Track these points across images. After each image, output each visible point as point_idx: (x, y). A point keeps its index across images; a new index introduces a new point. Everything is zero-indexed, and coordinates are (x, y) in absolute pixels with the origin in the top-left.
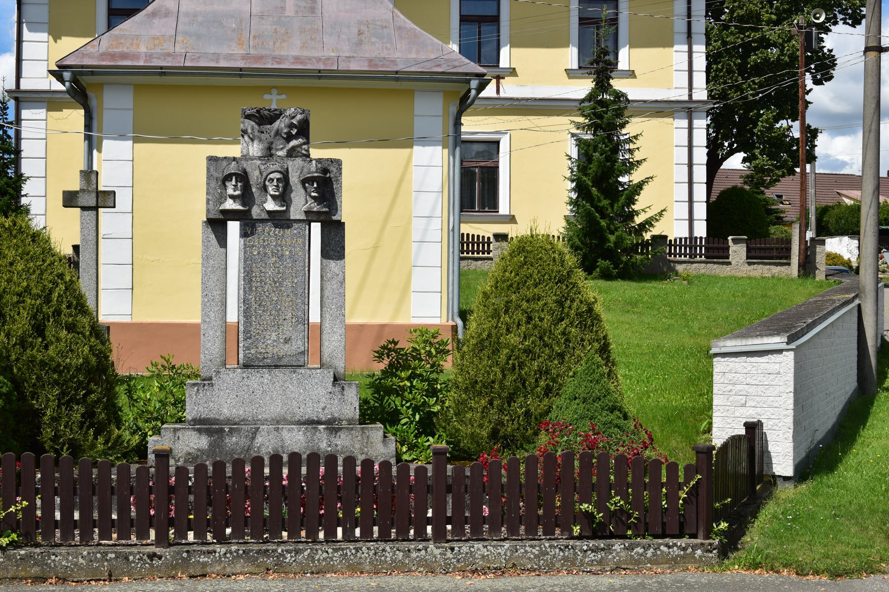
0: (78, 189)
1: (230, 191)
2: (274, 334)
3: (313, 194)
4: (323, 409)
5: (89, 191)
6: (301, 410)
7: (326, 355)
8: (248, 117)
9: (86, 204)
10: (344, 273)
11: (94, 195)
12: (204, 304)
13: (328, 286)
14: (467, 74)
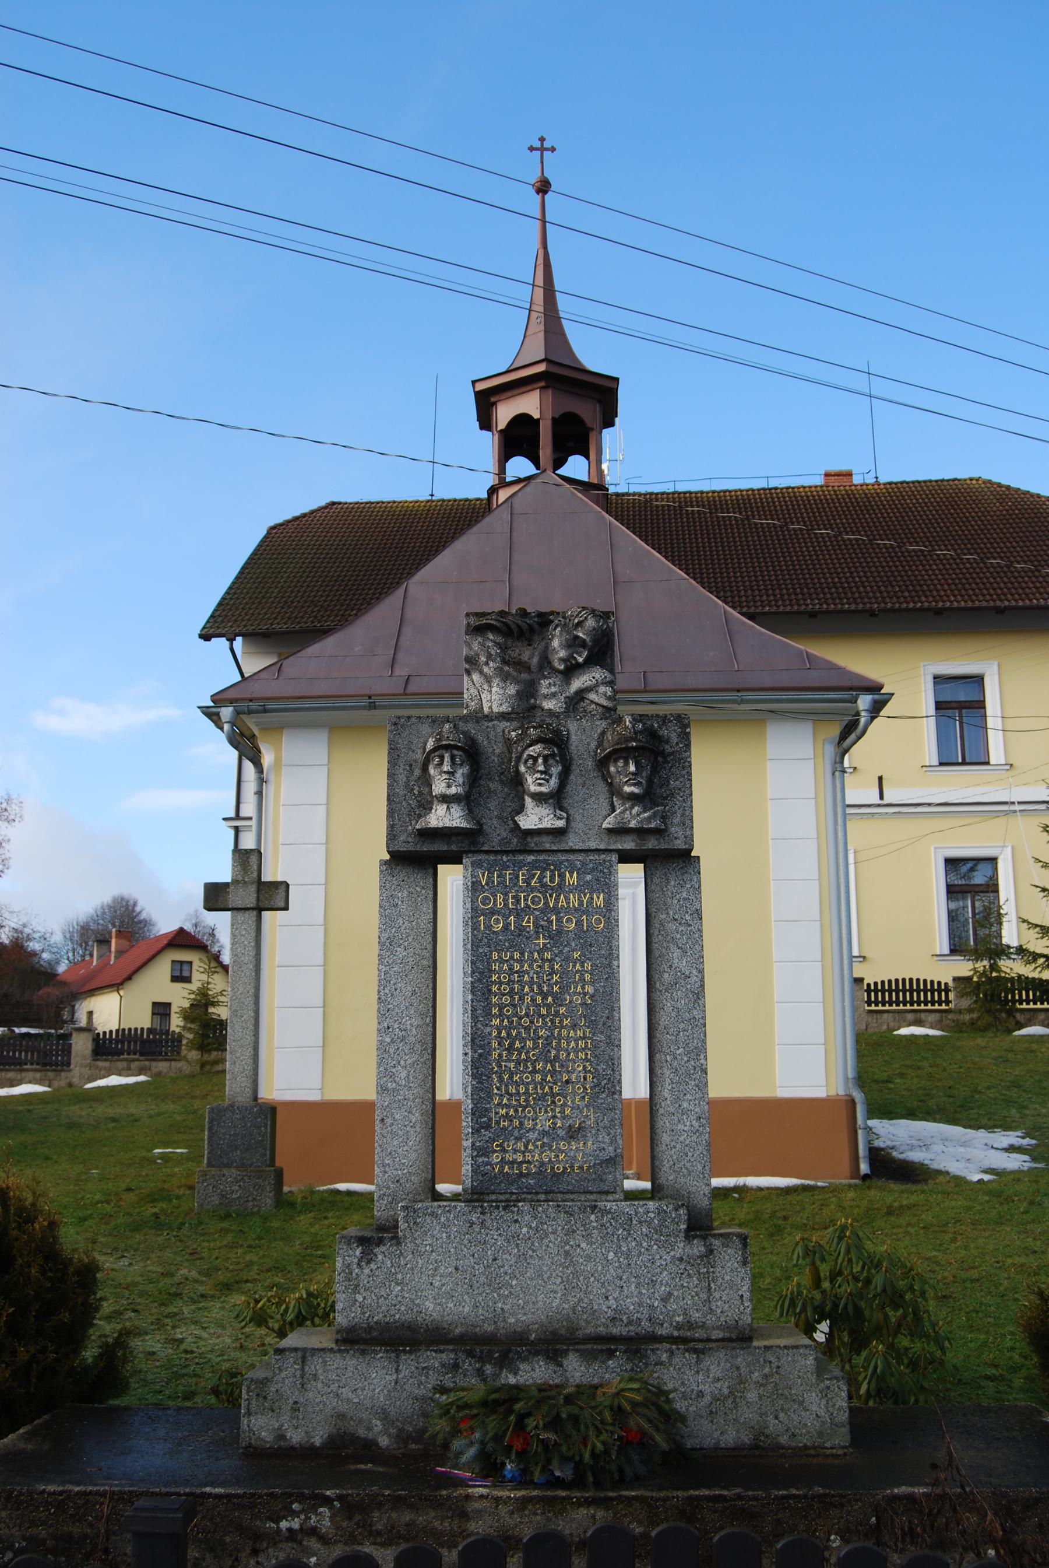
0: (229, 880)
1: (439, 787)
2: (542, 1116)
3: (627, 789)
4: (665, 1299)
5: (245, 882)
6: (612, 1302)
7: (666, 1165)
8: (478, 630)
9: (239, 904)
10: (701, 972)
11: (253, 888)
12: (383, 1049)
13: (667, 1004)
14: (851, 689)
